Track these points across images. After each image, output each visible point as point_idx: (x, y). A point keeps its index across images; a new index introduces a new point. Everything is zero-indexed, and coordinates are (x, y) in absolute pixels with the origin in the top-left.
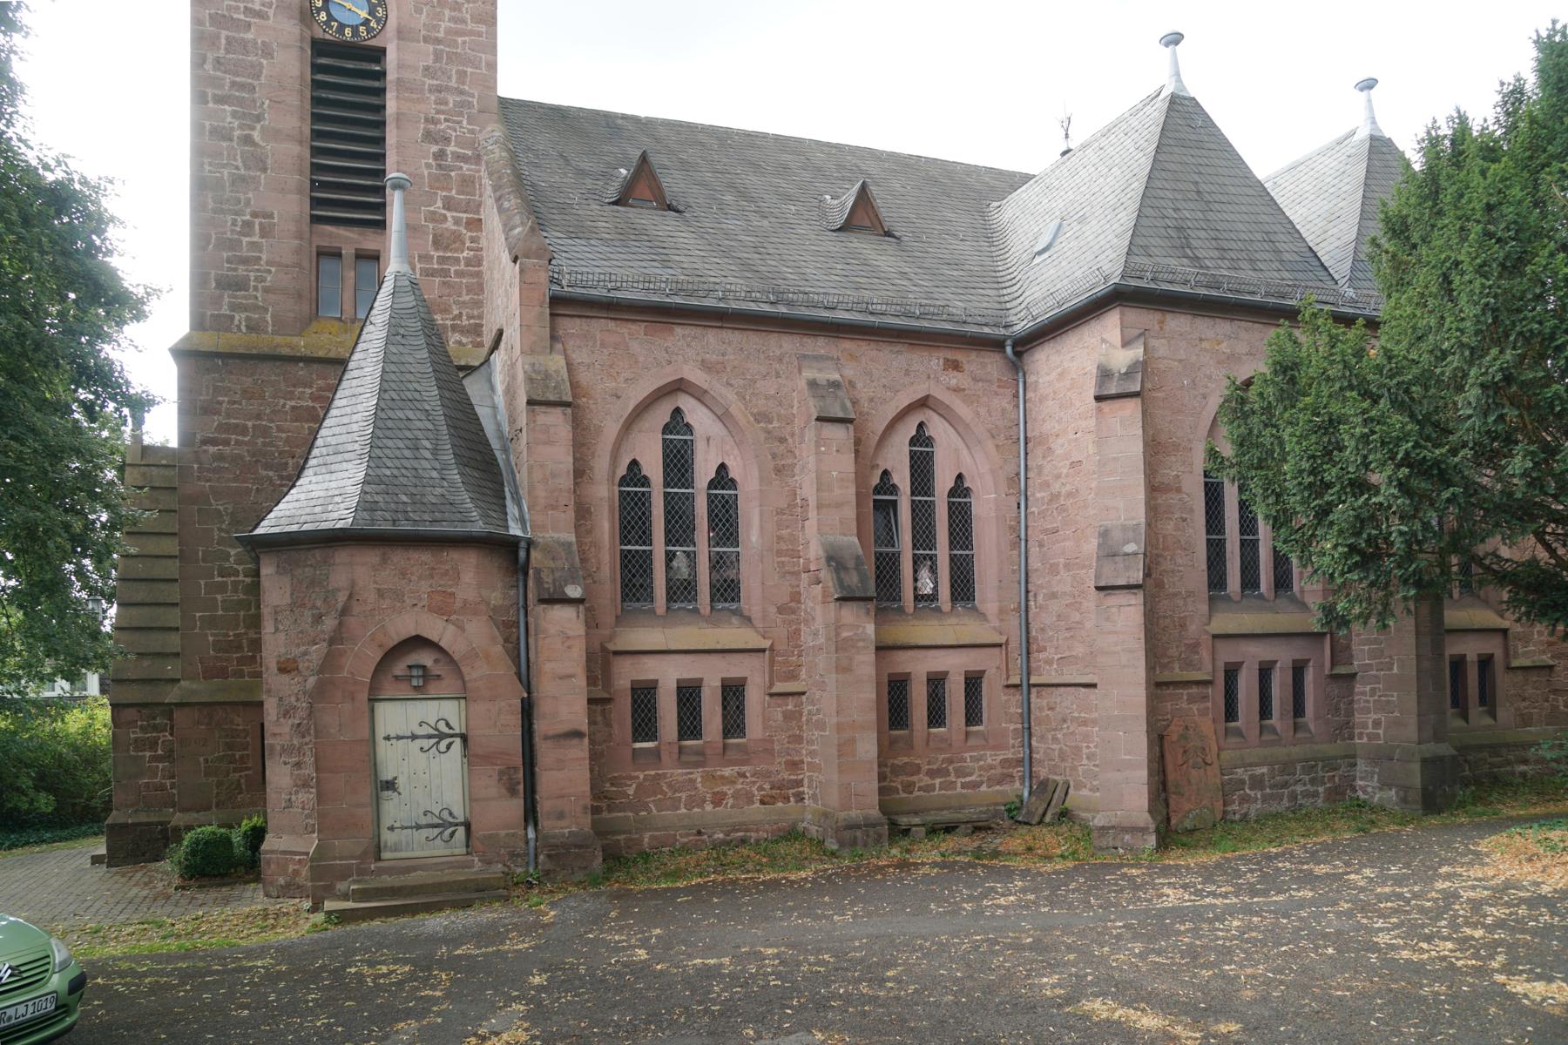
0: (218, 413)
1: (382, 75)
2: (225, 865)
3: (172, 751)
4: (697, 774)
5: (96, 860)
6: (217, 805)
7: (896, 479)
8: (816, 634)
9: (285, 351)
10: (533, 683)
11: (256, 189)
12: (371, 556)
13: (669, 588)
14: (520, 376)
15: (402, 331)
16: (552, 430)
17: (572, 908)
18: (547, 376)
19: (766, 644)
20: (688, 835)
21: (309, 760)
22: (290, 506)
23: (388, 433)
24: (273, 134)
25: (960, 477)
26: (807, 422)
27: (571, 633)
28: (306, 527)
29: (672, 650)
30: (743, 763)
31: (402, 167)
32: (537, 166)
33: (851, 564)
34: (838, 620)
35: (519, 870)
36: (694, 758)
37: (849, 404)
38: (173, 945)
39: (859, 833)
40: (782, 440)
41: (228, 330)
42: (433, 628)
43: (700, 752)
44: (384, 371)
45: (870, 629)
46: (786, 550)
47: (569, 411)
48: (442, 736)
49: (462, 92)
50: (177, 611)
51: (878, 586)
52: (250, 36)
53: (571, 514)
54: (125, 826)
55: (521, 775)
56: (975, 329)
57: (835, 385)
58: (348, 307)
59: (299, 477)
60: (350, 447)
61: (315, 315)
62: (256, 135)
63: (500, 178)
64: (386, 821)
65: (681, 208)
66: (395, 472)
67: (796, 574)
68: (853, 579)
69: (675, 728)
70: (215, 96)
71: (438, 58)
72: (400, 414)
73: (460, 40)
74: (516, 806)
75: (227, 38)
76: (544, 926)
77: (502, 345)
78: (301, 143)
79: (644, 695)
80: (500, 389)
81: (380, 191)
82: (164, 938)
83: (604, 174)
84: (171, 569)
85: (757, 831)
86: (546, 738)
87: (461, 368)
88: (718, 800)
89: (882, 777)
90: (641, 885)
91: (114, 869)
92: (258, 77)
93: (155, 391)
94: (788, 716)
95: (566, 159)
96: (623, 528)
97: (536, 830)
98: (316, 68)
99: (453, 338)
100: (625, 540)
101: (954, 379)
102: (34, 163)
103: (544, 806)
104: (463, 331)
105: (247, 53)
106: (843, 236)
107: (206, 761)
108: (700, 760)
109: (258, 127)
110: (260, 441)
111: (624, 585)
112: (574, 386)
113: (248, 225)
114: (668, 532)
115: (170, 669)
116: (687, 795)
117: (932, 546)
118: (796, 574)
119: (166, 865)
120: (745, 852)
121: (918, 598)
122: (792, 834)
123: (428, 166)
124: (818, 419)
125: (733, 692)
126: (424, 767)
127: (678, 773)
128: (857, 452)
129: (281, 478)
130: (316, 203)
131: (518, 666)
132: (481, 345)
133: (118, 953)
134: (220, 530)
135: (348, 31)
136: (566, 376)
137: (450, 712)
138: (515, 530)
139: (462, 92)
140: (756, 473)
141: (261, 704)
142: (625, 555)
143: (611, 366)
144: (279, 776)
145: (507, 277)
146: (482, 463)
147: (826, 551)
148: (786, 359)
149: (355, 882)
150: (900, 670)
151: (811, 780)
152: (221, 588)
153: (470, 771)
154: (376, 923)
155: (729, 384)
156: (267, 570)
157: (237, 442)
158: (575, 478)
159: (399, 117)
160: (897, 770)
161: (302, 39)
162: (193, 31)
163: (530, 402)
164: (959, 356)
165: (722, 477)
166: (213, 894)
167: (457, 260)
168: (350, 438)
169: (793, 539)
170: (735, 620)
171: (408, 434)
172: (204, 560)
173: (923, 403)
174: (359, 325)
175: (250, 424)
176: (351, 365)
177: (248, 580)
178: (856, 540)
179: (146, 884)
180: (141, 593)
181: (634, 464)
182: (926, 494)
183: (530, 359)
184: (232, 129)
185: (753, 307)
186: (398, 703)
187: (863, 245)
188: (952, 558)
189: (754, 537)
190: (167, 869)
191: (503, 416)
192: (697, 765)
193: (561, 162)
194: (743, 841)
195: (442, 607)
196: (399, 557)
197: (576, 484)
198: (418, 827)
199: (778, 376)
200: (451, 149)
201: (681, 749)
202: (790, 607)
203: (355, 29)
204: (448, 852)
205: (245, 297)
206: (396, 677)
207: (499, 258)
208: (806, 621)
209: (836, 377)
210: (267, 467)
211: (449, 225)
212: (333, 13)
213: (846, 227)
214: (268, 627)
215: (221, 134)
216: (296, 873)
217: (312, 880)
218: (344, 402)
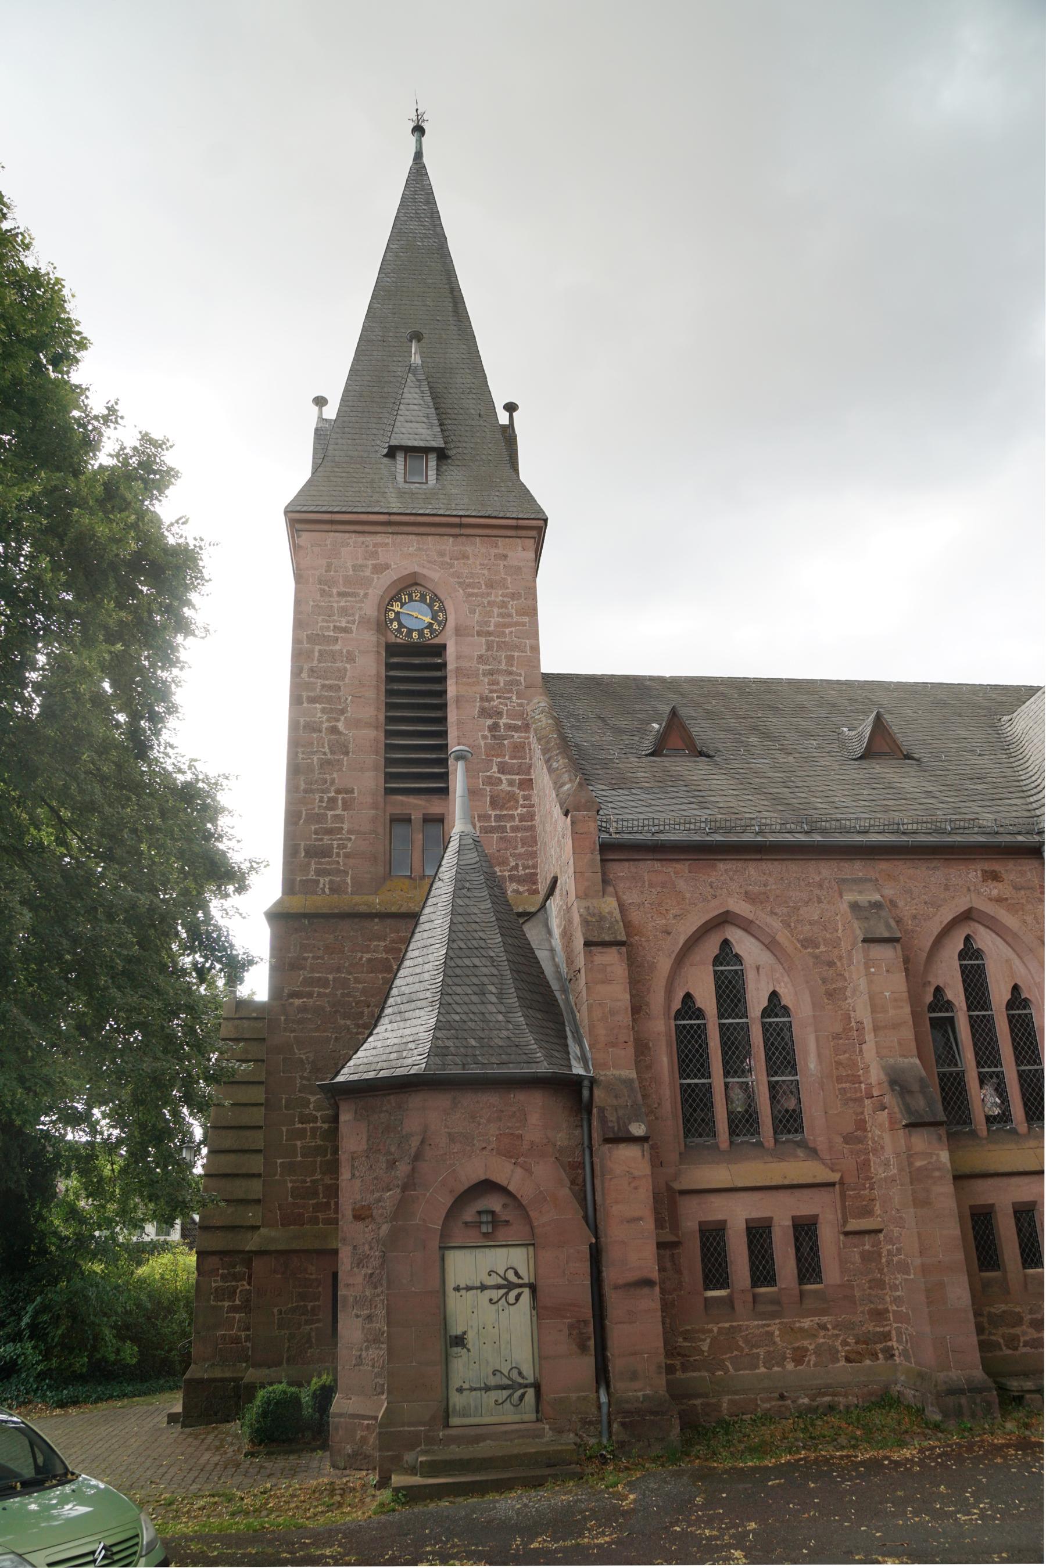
0: (303, 968)
1: (443, 666)
2: (291, 1431)
3: (248, 1300)
4: (775, 1327)
5: (172, 1418)
7: (950, 995)
8: (887, 1164)
9: (363, 909)
10: (601, 1227)
11: (340, 770)
12: (442, 1100)
13: (731, 1122)
14: (577, 919)
15: (467, 885)
16: (609, 969)
17: (652, 1491)
18: (602, 918)
19: (835, 1177)
20: (771, 1399)
21: (381, 1312)
22: (368, 1053)
23: (457, 980)
24: (356, 724)
25: (1016, 988)
26: (854, 944)
27: (636, 1173)
28: (382, 1074)
29: (740, 1189)
30: (824, 1312)
31: (463, 741)
32: (579, 728)
33: (916, 1087)
34: (909, 1148)
35: (592, 1441)
36: (770, 1308)
37: (893, 923)
38: (242, 1523)
39: (963, 1400)
40: (831, 964)
41: (315, 893)
42: (503, 1172)
43: (776, 1301)
44: (452, 922)
45: (944, 1156)
46: (846, 1075)
47: (624, 949)
48: (510, 1286)
49: (510, 673)
50: (260, 1158)
51: (946, 1110)
52: (337, 647)
53: (630, 1050)
54: (200, 1381)
55: (591, 1329)
56: (1009, 839)
57: (877, 905)
58: (417, 865)
59: (375, 1026)
60: (422, 995)
61: (388, 875)
62: (341, 725)
63: (548, 742)
64: (456, 1382)
65: (712, 753)
66: (464, 1017)
67: (859, 1101)
68: (919, 1103)
69: (747, 1268)
70: (308, 697)
71: (489, 647)
72: (467, 962)
73: (507, 631)
74: (588, 1363)
75: (320, 651)
76: (625, 1514)
77: (557, 891)
78: (377, 728)
79: (713, 1236)
80: (556, 932)
81: (444, 762)
82: (233, 1514)
83: (639, 730)
84: (257, 1116)
85: (846, 1395)
86: (616, 1287)
87: (520, 915)
88: (799, 1357)
89: (980, 1329)
90: (723, 1464)
91: (188, 1430)
92: (343, 679)
93: (255, 953)
94: (866, 1257)
95: (603, 720)
96: (681, 1061)
97: (609, 1394)
98: (389, 666)
99: (511, 888)
100: (684, 1073)
101: (995, 889)
102: (170, 768)
103: (617, 1365)
104: (519, 880)
105: (334, 661)
106: (865, 764)
108: (776, 1308)
109: (342, 718)
110: (339, 992)
111: (686, 1121)
112: (627, 925)
113: (332, 801)
114: (725, 1063)
115: (252, 1216)
116: (772, 1352)
117: (998, 1063)
118: (859, 1101)
119: (235, 1427)
120: (834, 1420)
121: (990, 1120)
122: (886, 1400)
123: (484, 737)
124: (865, 941)
125: (805, 1231)
126: (494, 1318)
127: (754, 1325)
128: (906, 970)
129: (358, 1026)
130: (389, 777)
131: (585, 1208)
132: (536, 892)
133: (189, 1531)
134: (302, 1078)
135: (415, 635)
136: (619, 917)
137: (514, 1259)
138: (578, 1070)
139: (510, 673)
140: (807, 998)
141: (335, 1252)
142: (685, 1089)
143: (660, 904)
144: (351, 1329)
145: (559, 829)
146: (544, 1002)
147: (887, 1074)
148: (826, 884)
149: (425, 1452)
150: (981, 1201)
151: (899, 1334)
152: (301, 1134)
153: (539, 1327)
154: (444, 1504)
155: (773, 913)
156: (345, 1117)
157: (319, 995)
158: (633, 1015)
159: (458, 699)
160: (996, 1320)
161: (378, 645)
162: (294, 649)
163: (587, 944)
164: (996, 866)
165: (775, 1005)
166: (281, 1463)
167: (512, 817)
168: (422, 986)
169: (853, 1064)
170: (800, 1153)
171: (475, 980)
173: (967, 916)
174: (426, 882)
175: (331, 977)
176: (423, 919)
177: (326, 1126)
178: (917, 1061)
179: (217, 1449)
180: (229, 1141)
181: (688, 996)
182: (983, 1009)
183: (585, 903)
184: (322, 722)
185: (789, 837)
186: (467, 1252)
187: (885, 770)
188: (1021, 1075)
189: (813, 1064)
190: (238, 1431)
191: (561, 957)
192: (774, 1315)
193: (600, 723)
194: (831, 1408)
195: (511, 1151)
196: (469, 1100)
197: (634, 1020)
198: (487, 1389)
199: (820, 901)
200: (503, 721)
201: (755, 1296)
202: (856, 1136)
203: (421, 633)
204: (516, 1418)
205: (329, 863)
206: (466, 1223)
207: (550, 813)
208: (875, 1151)
209: (877, 897)
210: (346, 1016)
211: (504, 786)
212: (403, 621)
213: (867, 755)
214: (345, 1174)
215: (312, 727)
216: (364, 1440)
217: (380, 1450)
218: (416, 953)
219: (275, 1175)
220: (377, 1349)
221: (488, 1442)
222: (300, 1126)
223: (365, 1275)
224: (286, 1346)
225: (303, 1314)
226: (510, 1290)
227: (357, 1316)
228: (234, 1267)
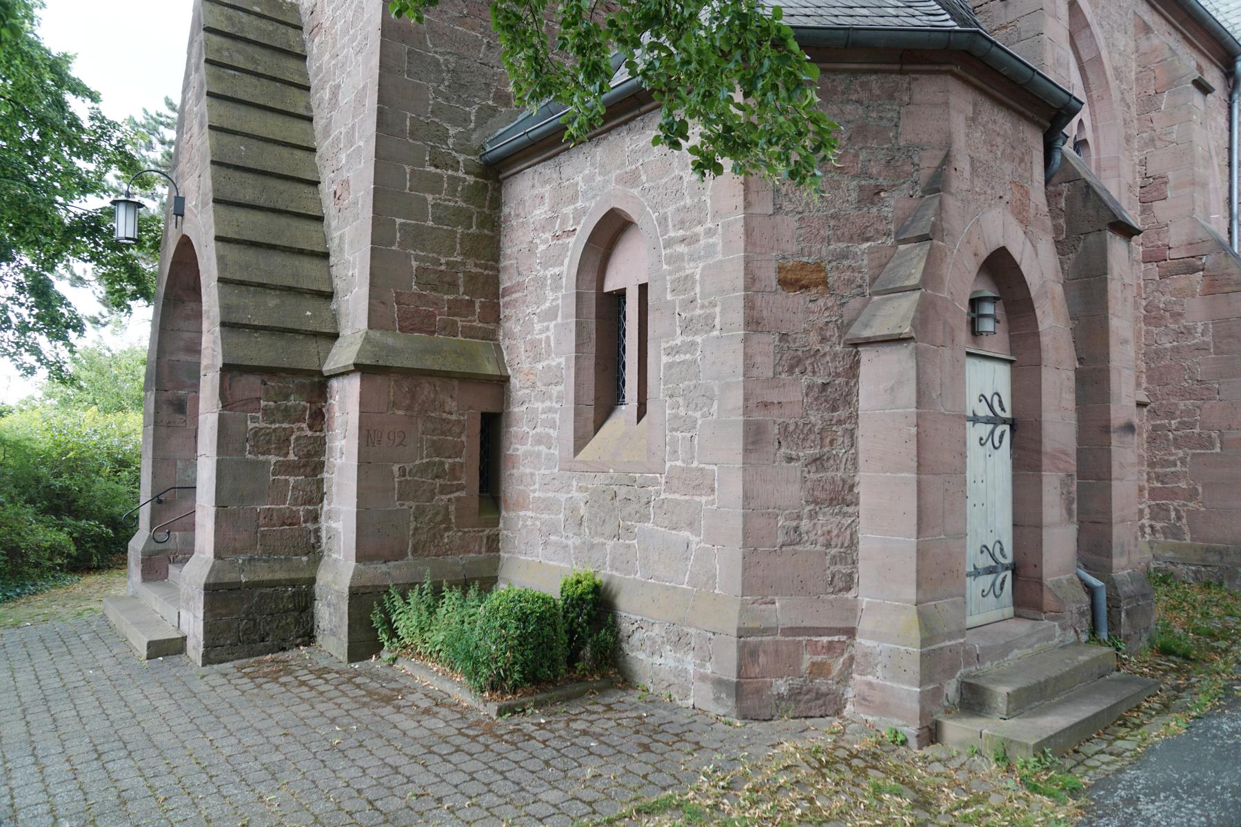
6: (415, 551)
107: (403, 472)
134: (438, 92)
152: (434, 184)
172: (412, 134)
177: (471, 179)
219: (392, 244)
220: (834, 515)
221: (1016, 651)
222: (432, 169)
223: (810, 387)
224: (412, 526)
225: (437, 477)
226: (996, 425)
227: (790, 459)
228: (286, 397)
